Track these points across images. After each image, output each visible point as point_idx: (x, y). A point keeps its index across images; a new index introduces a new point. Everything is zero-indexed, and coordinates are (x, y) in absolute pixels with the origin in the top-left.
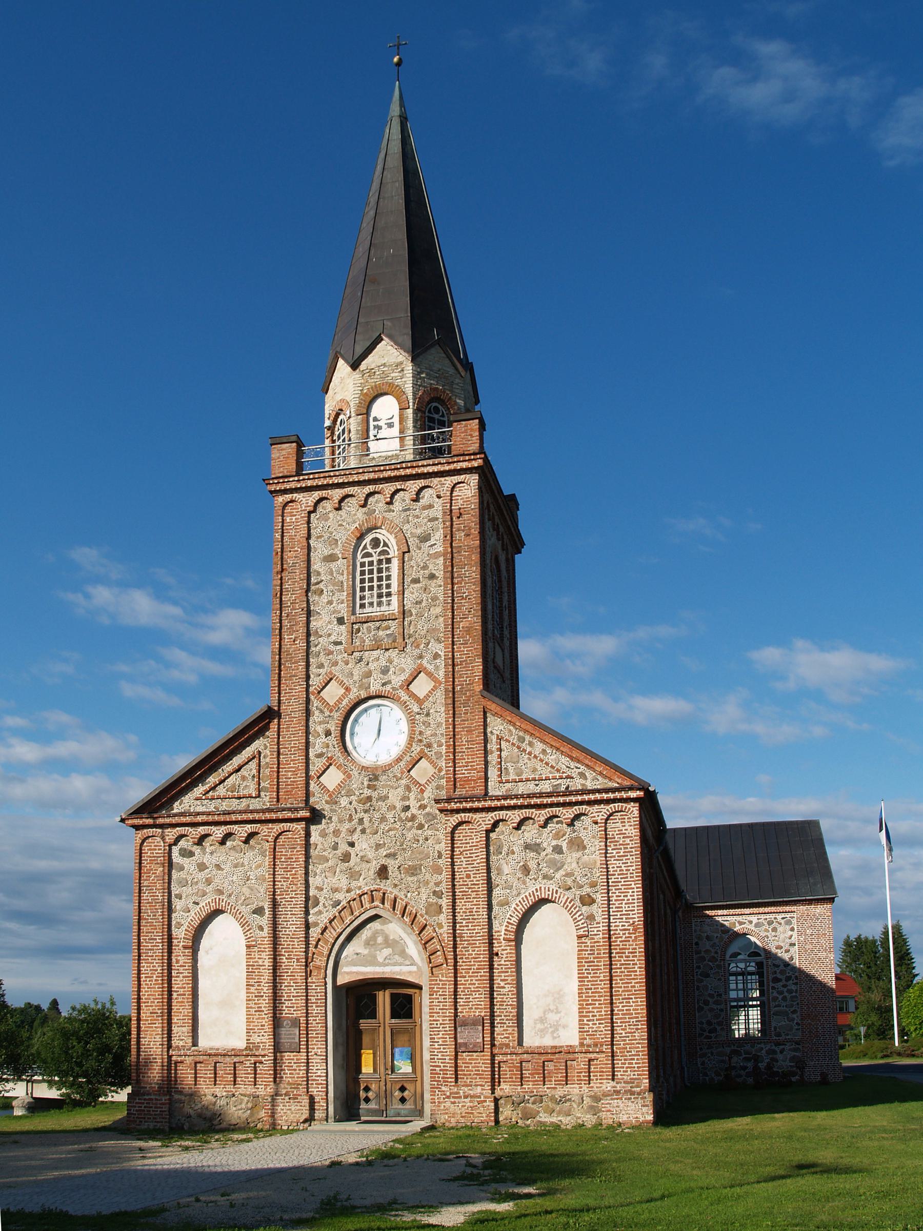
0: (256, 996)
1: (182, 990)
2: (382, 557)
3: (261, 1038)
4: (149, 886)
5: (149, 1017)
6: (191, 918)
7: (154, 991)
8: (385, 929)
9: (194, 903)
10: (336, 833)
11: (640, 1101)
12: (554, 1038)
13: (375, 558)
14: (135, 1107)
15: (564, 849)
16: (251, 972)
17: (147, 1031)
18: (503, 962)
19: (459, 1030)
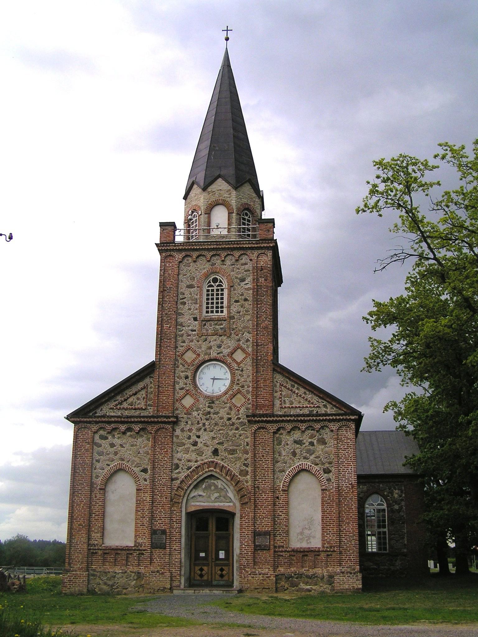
2: (219, 288)
3: (143, 540)
8: (216, 483)
9: (107, 465)
10: (190, 430)
12: (308, 543)
13: (215, 288)
14: (67, 578)
15: (315, 444)
19: (256, 538)
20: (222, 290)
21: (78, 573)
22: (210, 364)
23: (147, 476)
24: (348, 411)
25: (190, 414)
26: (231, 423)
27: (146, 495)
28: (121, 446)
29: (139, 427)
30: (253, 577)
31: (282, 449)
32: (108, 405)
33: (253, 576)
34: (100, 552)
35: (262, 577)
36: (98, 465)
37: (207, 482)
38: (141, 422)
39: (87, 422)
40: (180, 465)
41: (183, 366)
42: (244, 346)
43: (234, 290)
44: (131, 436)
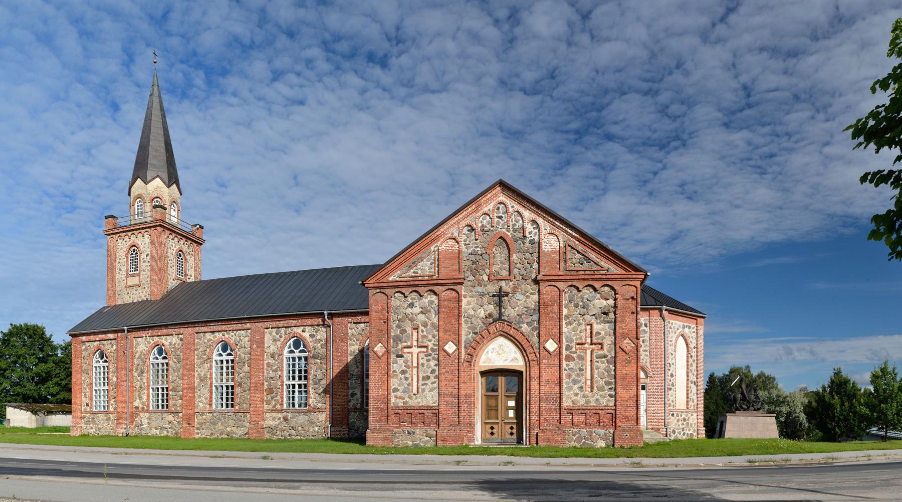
13: (134, 255)
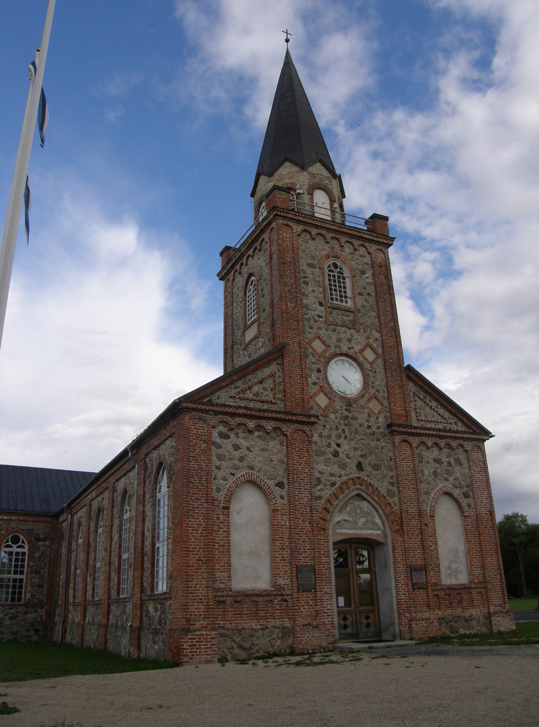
0: (280, 549)
1: (222, 542)
3: (285, 581)
4: (195, 457)
5: (195, 563)
6: (229, 485)
7: (200, 542)
8: (361, 505)
9: (231, 474)
10: (329, 437)
11: (508, 617)
12: (456, 579)
14: (188, 642)
15: (453, 464)
16: (276, 530)
17: (194, 575)
18: (430, 530)
19: (413, 574)
20: (344, 278)
21: (204, 633)
22: (337, 360)
23: (284, 493)
24: (478, 431)
25: (327, 416)
26: (371, 432)
27: (285, 518)
28: (248, 449)
29: (271, 426)
30: (416, 624)
31: (424, 467)
32: (227, 391)
33: (416, 622)
34: (229, 600)
35: (426, 623)
36: (220, 474)
37: (352, 503)
38: (275, 419)
39: (202, 411)
40: (323, 480)
41: (313, 356)
42: (375, 345)
43: (357, 281)
44: (259, 437)
